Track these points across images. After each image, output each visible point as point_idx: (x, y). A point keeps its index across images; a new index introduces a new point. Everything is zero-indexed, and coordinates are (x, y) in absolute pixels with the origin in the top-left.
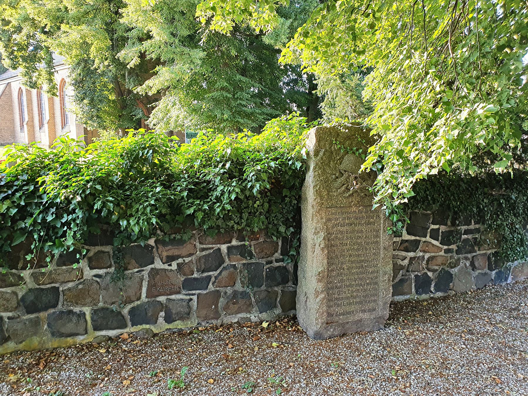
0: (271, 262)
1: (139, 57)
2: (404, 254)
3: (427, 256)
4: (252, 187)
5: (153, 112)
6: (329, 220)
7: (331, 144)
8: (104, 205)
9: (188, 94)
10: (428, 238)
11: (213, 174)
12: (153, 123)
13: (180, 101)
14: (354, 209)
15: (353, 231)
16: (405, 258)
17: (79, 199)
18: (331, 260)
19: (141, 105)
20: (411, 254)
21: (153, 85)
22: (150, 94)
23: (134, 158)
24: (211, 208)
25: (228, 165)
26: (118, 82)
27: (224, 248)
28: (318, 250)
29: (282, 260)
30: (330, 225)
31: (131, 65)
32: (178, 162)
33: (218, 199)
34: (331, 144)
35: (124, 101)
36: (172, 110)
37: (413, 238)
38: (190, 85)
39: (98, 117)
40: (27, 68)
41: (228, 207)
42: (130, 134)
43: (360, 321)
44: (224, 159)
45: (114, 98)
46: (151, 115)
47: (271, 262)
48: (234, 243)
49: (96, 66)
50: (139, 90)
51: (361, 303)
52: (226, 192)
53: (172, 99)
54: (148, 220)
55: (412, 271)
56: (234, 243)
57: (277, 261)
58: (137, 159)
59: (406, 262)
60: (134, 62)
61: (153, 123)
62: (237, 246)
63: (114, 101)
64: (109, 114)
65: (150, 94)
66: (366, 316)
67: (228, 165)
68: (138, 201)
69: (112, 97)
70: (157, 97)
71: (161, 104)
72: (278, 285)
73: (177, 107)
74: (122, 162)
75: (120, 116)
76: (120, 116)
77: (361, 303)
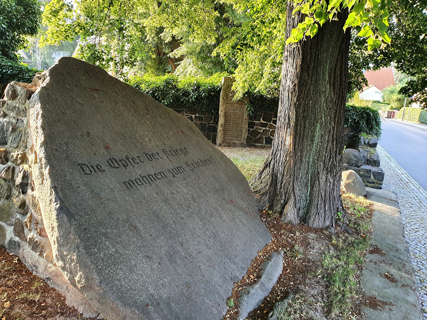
0: (210, 124)
1: (171, 37)
2: (261, 128)
3: (271, 130)
4: (202, 94)
5: (177, 68)
6: (226, 108)
7: (229, 82)
8: (158, 94)
9: (198, 58)
10: (272, 123)
11: (190, 89)
12: (177, 74)
13: (193, 63)
14: (235, 105)
15: (234, 113)
16: (261, 129)
17: (151, 92)
18: (226, 121)
19: (171, 62)
20: (264, 128)
21: (177, 53)
22: (176, 57)
23: (167, 83)
24: (189, 100)
25: (195, 87)
26: (158, 47)
27: (193, 116)
28: (222, 117)
29: (213, 124)
30: (227, 109)
31: (167, 41)
32: (180, 86)
33: (191, 97)
34: (229, 82)
35: (161, 59)
36: (188, 67)
37: (265, 122)
38: (199, 53)
39: (145, 68)
40: (108, 37)
41: (194, 100)
42: (166, 75)
43: (235, 143)
44: (194, 85)
45: (154, 57)
46: (176, 70)
47: (210, 124)
48: (197, 115)
49: (147, 39)
50: (171, 55)
51: (235, 137)
52: (193, 96)
53: (189, 60)
54: (170, 100)
55: (264, 135)
56: (197, 115)
57: (212, 124)
58: (168, 83)
59: (261, 131)
60: (168, 39)
61: (177, 74)
62: (198, 116)
63: (154, 59)
64: (151, 67)
65: (176, 57)
66: (237, 142)
67: (195, 87)
68: (167, 94)
69: (154, 56)
70: (181, 59)
71: (182, 63)
72: (212, 132)
73: (191, 65)
74: (163, 83)
75: (157, 69)
76: (157, 69)
77: (235, 137)
